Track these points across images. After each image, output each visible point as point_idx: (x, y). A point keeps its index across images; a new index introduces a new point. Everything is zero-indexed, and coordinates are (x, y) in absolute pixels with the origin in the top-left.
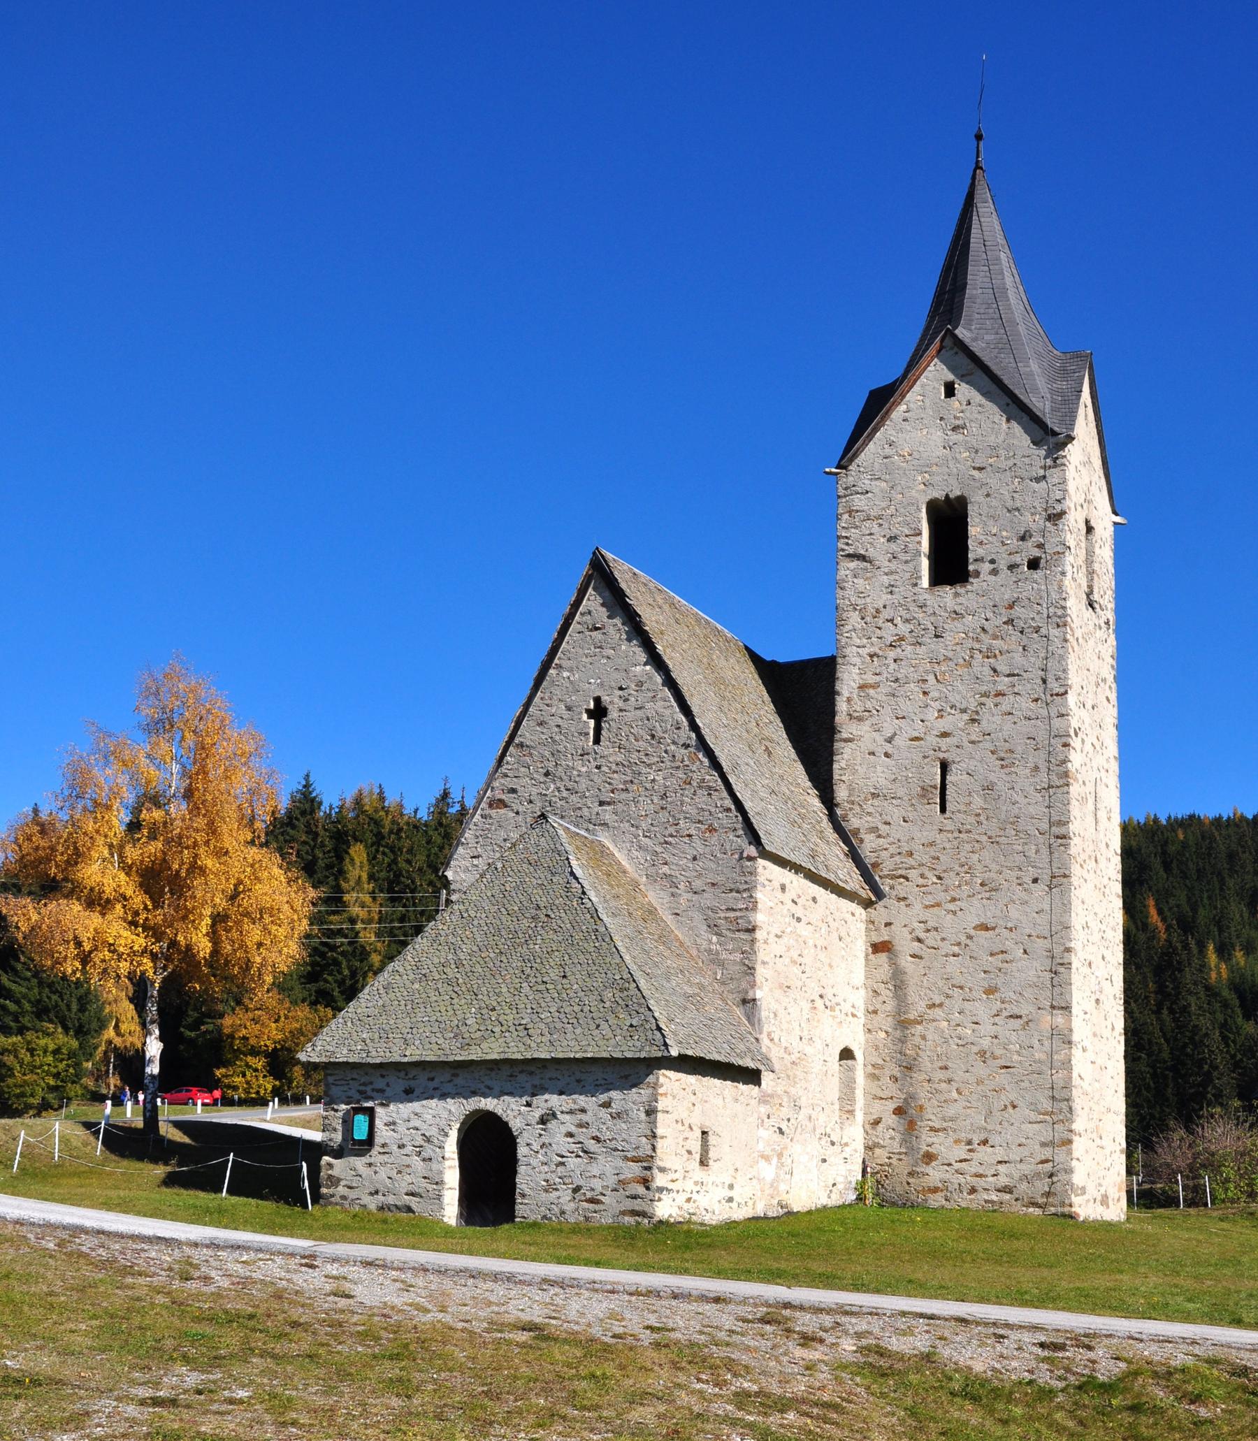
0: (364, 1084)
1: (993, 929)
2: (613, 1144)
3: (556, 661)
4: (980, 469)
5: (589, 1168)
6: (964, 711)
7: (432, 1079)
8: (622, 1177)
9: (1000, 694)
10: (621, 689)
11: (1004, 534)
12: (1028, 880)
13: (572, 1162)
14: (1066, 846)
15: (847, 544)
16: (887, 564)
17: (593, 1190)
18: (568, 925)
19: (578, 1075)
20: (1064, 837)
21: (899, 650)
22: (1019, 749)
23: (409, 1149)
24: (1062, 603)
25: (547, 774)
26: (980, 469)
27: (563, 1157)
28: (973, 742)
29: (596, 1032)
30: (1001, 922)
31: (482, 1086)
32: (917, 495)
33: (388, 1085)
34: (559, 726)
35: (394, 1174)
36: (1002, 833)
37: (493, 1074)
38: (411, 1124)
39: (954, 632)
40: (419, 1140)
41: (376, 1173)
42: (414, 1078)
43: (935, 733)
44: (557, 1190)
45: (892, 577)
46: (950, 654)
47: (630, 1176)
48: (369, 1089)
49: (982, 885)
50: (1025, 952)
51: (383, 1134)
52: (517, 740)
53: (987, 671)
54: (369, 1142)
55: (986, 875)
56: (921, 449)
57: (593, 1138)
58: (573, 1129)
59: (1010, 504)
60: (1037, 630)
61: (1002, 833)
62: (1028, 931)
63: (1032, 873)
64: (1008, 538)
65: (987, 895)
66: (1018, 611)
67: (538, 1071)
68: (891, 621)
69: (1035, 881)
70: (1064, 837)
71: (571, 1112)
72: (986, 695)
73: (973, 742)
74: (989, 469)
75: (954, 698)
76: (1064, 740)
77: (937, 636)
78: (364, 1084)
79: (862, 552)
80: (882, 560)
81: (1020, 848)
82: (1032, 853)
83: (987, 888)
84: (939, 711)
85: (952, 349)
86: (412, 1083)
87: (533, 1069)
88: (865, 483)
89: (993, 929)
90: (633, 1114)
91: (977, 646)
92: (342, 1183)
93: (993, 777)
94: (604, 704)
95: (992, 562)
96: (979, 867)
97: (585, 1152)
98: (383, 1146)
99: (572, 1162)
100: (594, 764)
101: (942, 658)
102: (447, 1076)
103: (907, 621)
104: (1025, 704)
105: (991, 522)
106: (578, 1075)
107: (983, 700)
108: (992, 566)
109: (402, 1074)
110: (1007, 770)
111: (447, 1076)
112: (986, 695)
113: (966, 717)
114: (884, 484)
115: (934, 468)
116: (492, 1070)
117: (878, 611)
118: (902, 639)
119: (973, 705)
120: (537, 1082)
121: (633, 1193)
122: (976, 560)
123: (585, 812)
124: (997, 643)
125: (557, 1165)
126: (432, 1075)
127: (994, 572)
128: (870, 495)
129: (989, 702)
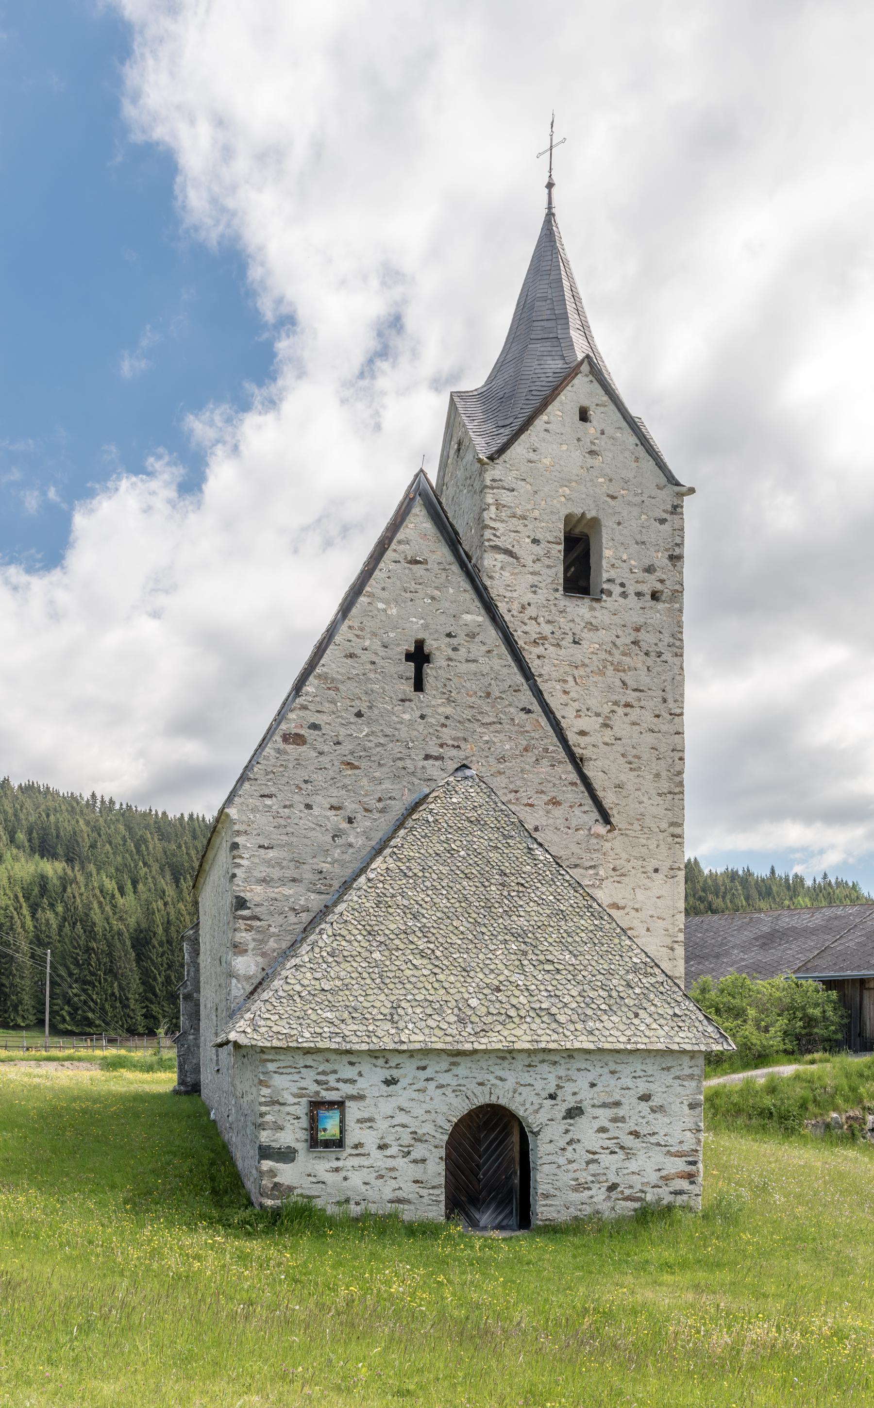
0: (324, 1073)
1: (623, 908)
2: (653, 1140)
3: (367, 589)
4: (613, 498)
5: (627, 1164)
6: (598, 715)
7: (424, 1068)
8: (664, 1173)
9: (627, 705)
10: (449, 635)
11: (633, 562)
12: (650, 869)
13: (606, 1159)
14: (681, 844)
15: (495, 535)
16: (531, 564)
17: (631, 1187)
18: (551, 898)
19: (613, 1066)
20: (679, 836)
21: (541, 648)
22: (645, 756)
23: (393, 1150)
24: (679, 635)
25: (359, 715)
26: (613, 498)
27: (594, 1153)
28: (606, 744)
29: (636, 1021)
30: (630, 904)
31: (491, 1077)
32: (558, 506)
33: (360, 1074)
34: (373, 663)
35: (371, 1178)
36: (630, 827)
37: (506, 1064)
38: (395, 1121)
39: (591, 642)
40: (407, 1139)
41: (345, 1179)
42: (397, 1066)
43: (575, 730)
44: (589, 1189)
45: (536, 578)
46: (587, 661)
47: (673, 1171)
48: (331, 1078)
49: (614, 869)
50: (648, 930)
51: (354, 1134)
52: (318, 670)
53: (618, 683)
54: (339, 1143)
55: (618, 862)
56: (562, 463)
57: (631, 1133)
58: (607, 1124)
59: (639, 538)
60: (659, 654)
61: (630, 827)
62: (651, 913)
63: (655, 864)
64: (635, 567)
65: (618, 879)
66: (642, 635)
67: (562, 1061)
68: (535, 619)
69: (656, 871)
70: (679, 836)
71: (604, 1105)
72: (616, 703)
73: (606, 744)
74: (620, 499)
75: (593, 703)
76: (680, 754)
77: (575, 642)
78: (324, 1073)
79: (509, 547)
80: (528, 560)
81: (644, 841)
82: (653, 847)
83: (618, 873)
84: (578, 711)
85: (587, 376)
86: (395, 1073)
87: (557, 1058)
88: (509, 479)
89: (623, 908)
90: (676, 1107)
91: (610, 659)
92: (296, 1192)
93: (623, 777)
94: (426, 650)
95: (622, 585)
96: (611, 853)
97: (622, 1148)
98: (356, 1147)
99: (606, 1159)
100: (418, 714)
101: (580, 664)
102: (444, 1065)
103: (549, 622)
104: (647, 718)
105: (621, 549)
106: (613, 1066)
107: (615, 708)
108: (622, 589)
109: (381, 1062)
110: (636, 773)
111: (444, 1065)
112: (616, 703)
113: (600, 720)
114: (528, 486)
115: (574, 484)
116: (504, 1058)
117: (523, 607)
118: (545, 638)
119: (606, 709)
120: (562, 1073)
121: (678, 1188)
122: (609, 580)
123: (408, 763)
124: (627, 660)
125: (588, 1163)
126: (423, 1063)
127: (624, 595)
128: (515, 493)
129: (620, 711)
